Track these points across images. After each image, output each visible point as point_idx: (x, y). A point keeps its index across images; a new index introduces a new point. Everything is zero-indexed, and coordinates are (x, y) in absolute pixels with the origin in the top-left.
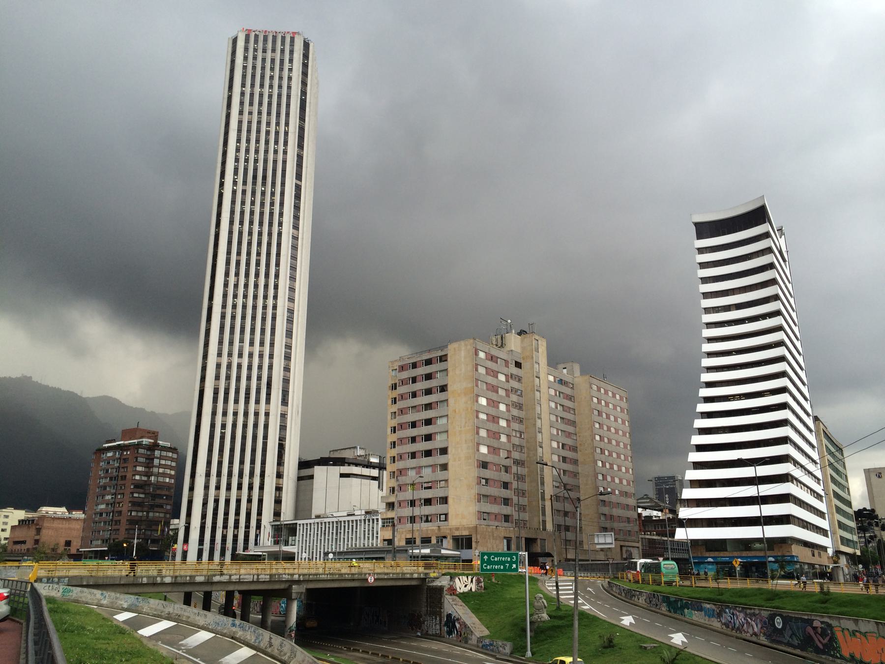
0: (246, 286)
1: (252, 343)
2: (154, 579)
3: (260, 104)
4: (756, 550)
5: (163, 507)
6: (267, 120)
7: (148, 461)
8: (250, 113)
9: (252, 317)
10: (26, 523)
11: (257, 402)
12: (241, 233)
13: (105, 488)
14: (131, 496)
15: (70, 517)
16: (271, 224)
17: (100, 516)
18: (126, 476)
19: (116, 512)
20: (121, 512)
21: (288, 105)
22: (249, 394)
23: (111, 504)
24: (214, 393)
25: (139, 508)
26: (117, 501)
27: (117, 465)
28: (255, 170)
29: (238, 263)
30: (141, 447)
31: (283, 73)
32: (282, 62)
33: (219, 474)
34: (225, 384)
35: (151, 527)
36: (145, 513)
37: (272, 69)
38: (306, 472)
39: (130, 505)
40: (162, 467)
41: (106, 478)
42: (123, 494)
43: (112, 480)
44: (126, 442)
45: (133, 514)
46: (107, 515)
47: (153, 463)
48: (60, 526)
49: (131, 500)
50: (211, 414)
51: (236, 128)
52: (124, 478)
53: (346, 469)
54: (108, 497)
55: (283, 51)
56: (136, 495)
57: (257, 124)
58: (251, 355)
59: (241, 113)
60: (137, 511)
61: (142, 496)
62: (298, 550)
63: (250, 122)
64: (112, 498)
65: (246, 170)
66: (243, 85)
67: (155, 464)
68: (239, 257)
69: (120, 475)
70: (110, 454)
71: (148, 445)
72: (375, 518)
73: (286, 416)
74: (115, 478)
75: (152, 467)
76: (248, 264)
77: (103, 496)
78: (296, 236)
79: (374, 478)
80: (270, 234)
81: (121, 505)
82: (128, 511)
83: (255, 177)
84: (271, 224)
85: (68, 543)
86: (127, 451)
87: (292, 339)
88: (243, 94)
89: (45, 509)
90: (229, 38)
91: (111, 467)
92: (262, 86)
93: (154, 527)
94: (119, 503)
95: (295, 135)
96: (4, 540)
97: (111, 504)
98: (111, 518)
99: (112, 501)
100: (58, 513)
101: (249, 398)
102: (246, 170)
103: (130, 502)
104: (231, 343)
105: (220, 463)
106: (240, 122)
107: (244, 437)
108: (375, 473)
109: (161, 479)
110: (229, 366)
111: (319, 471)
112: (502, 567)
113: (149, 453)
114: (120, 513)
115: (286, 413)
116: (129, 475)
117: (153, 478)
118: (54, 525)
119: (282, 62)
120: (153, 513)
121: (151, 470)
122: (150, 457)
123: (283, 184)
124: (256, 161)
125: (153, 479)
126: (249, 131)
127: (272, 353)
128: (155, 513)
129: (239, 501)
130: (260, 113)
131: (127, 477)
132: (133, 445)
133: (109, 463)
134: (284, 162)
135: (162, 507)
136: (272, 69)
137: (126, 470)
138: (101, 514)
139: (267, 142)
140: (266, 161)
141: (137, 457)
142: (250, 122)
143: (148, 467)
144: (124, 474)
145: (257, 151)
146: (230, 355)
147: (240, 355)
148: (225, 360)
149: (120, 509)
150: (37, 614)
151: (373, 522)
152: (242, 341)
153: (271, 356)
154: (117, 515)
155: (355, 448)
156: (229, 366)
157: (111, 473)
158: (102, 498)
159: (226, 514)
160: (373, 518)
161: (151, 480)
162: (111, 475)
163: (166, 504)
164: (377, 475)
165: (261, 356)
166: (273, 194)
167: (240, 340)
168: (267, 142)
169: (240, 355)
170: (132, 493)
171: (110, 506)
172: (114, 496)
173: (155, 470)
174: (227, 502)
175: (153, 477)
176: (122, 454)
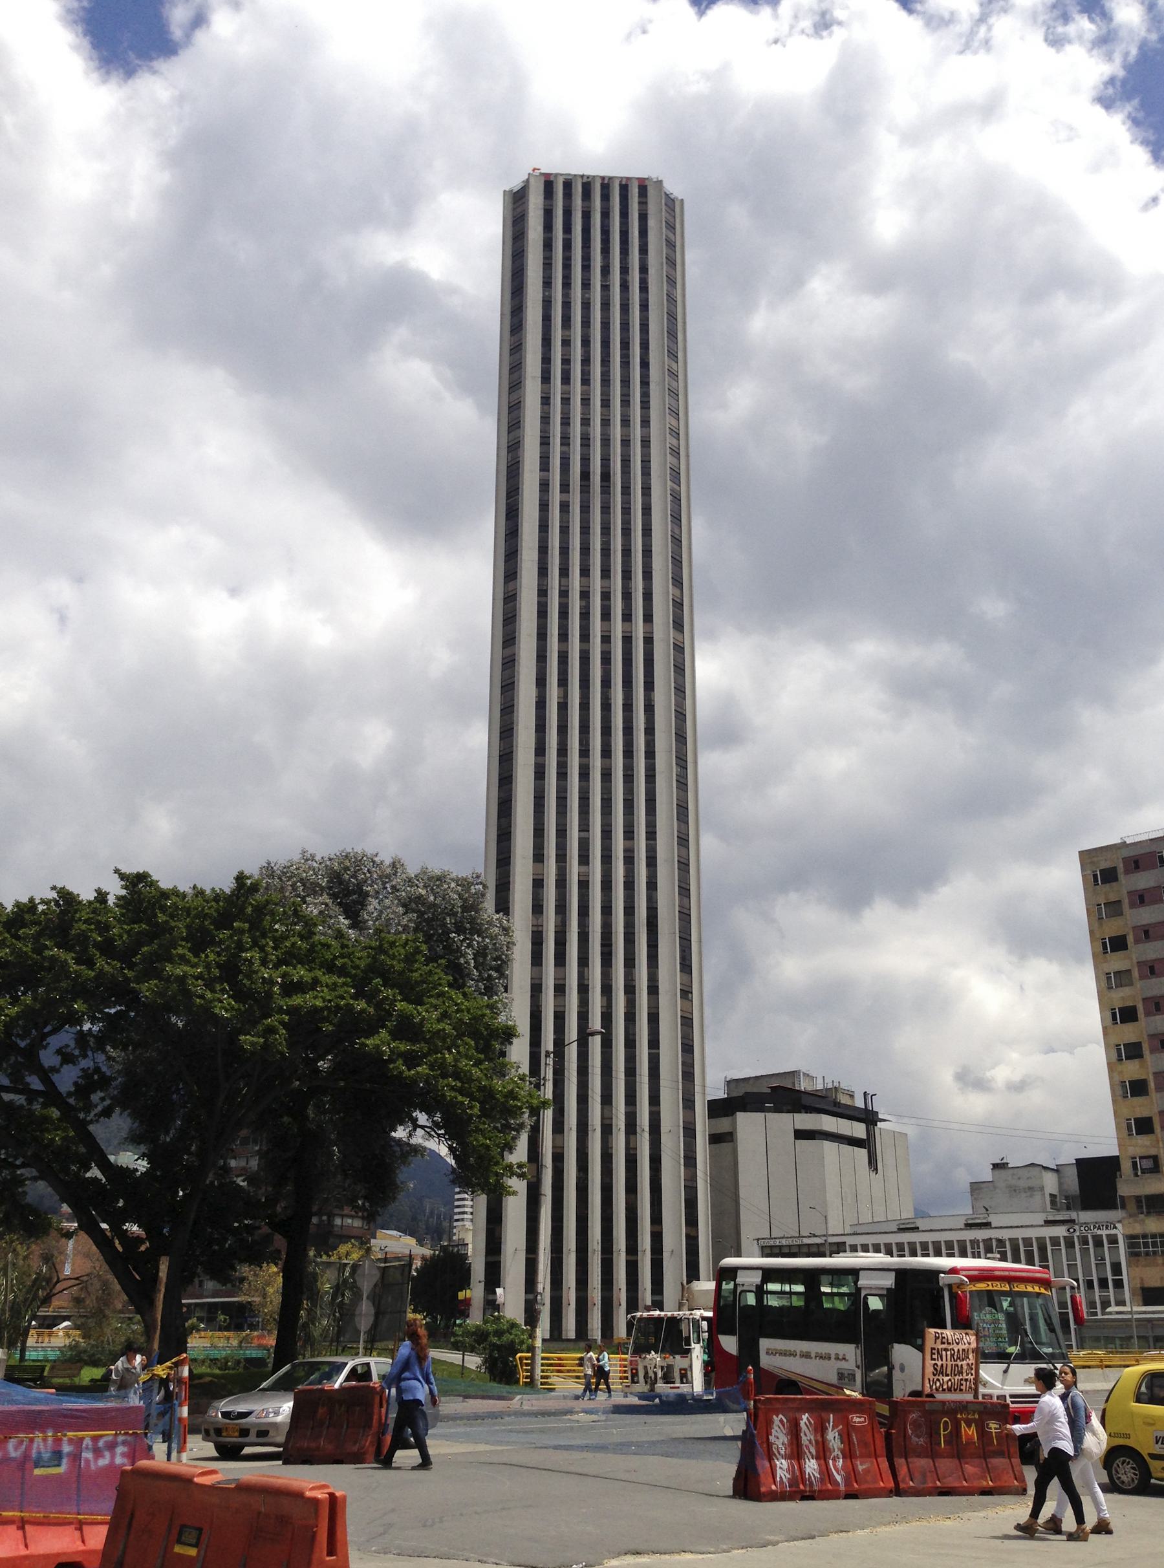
9: (557, 830)
24: (533, 944)
28: (586, 460)
36: (325, 1218)
38: (723, 1125)
53: (806, 1121)
72: (1104, 1232)
73: (690, 995)
78: (678, 600)
83: (585, 476)
105: (584, 827)
111: (748, 1124)
150: (330, 859)
151: (1085, 1252)
160: (1099, 1232)
164: (863, 1136)
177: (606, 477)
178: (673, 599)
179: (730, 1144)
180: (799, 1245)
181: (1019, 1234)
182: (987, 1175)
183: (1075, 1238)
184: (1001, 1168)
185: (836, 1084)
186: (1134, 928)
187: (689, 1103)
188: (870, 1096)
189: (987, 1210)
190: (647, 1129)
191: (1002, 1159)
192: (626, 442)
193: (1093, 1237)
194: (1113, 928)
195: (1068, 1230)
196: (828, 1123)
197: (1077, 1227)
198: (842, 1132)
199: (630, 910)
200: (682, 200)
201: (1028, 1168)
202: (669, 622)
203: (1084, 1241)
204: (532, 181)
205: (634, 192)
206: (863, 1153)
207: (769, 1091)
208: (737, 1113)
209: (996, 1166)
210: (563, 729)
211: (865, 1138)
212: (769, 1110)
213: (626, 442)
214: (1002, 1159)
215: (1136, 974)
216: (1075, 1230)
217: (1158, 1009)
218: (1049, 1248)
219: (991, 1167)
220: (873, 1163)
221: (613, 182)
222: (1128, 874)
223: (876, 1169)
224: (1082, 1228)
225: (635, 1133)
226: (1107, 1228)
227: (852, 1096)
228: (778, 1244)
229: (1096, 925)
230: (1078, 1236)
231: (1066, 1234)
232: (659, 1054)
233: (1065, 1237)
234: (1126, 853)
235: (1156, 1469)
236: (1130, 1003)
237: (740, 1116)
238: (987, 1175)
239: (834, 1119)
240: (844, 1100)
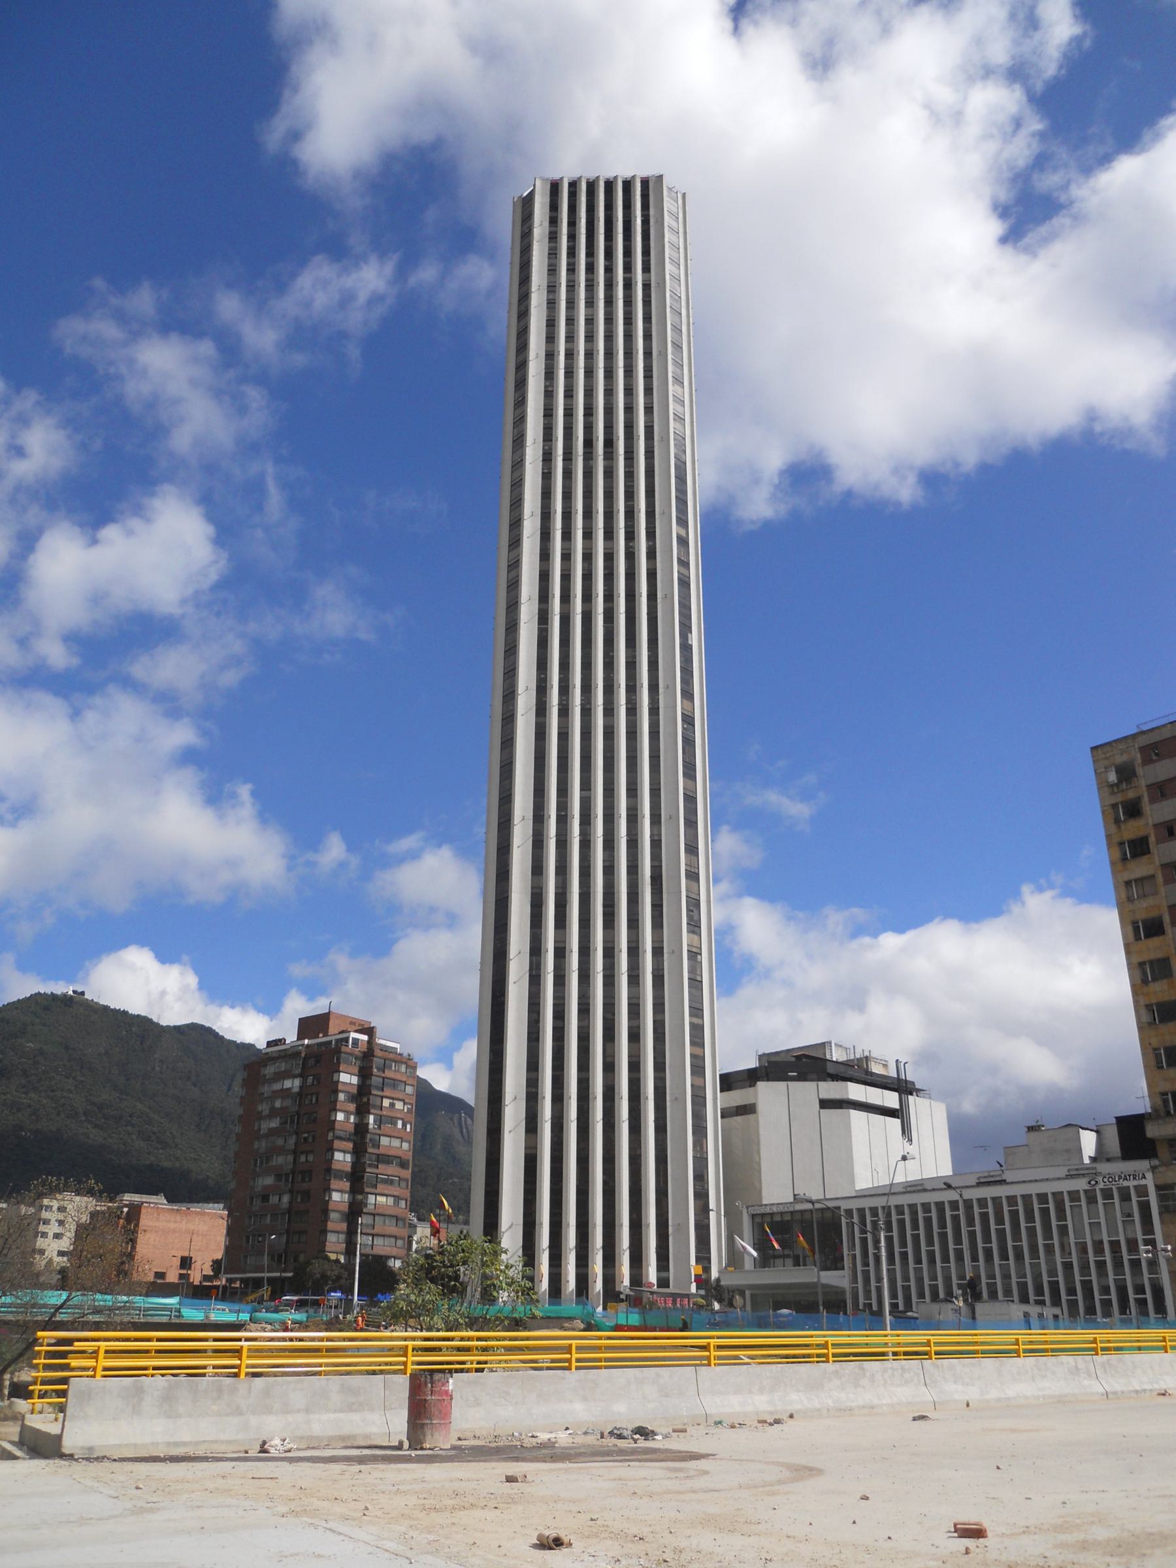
2: (812, 1214)
4: (976, 1269)
17: (262, 1202)
29: (590, 321)
38: (737, 1097)
48: (172, 1225)
53: (830, 1089)
62: (854, 1279)
72: (1131, 1183)
73: (699, 957)
83: (589, 443)
85: (186, 1262)
96: (58, 1256)
107: (569, 413)
108: (891, 1099)
111: (767, 1094)
118: (157, 1224)
154: (299, 1200)
160: (1126, 1183)
177: (609, 443)
180: (791, 1212)
181: (1034, 1189)
182: (1022, 1137)
183: (1098, 1191)
184: (1036, 1130)
185: (866, 1054)
186: (1155, 826)
187: (698, 1069)
188: (902, 1064)
189: (1001, 1166)
191: (1037, 1121)
193: (1119, 1189)
194: (1133, 829)
195: (1089, 1183)
196: (856, 1091)
197: (1100, 1179)
199: (633, 869)
201: (1065, 1129)
203: (1108, 1194)
206: (895, 1123)
207: (793, 1059)
208: (758, 1083)
209: (1031, 1129)
210: (565, 689)
211: (897, 1106)
214: (1037, 1121)
215: (1160, 878)
216: (1097, 1182)
217: (1171, 833)
218: (1067, 1204)
219: (1026, 1129)
220: (906, 1131)
222: (1153, 803)
223: (910, 1140)
224: (1105, 1180)
226: (1134, 1178)
227: (885, 1066)
229: (1113, 829)
230: (1102, 1190)
231: (1087, 1187)
233: (1086, 1191)
234: (1144, 741)
236: (1154, 914)
237: (760, 1085)
238: (1022, 1137)
239: (862, 1087)
240: (876, 1069)
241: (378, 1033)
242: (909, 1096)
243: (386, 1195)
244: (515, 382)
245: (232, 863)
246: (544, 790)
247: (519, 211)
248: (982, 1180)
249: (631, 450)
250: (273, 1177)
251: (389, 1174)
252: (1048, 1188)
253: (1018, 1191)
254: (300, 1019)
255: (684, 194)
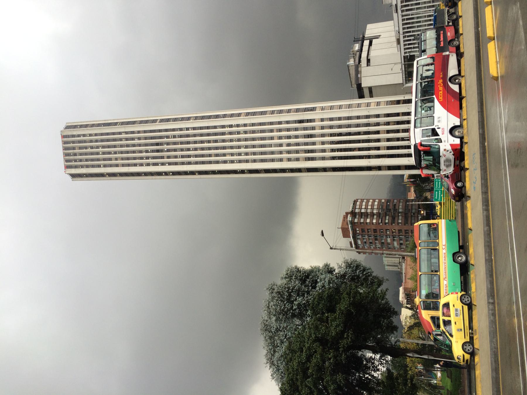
0: (232, 147)
1: (272, 138)
3: (109, 153)
5: (395, 204)
6: (119, 148)
7: (363, 217)
8: (116, 159)
10: (409, 300)
11: (313, 128)
12: (196, 156)
13: (383, 243)
14: (388, 224)
15: (405, 273)
16: (188, 136)
18: (374, 230)
19: (399, 234)
20: (399, 230)
21: (108, 134)
22: (308, 135)
23: (394, 237)
25: (396, 218)
26: (391, 234)
27: (366, 237)
28: (153, 151)
29: (217, 155)
30: (353, 221)
31: (87, 140)
32: (80, 142)
33: (369, 149)
34: (301, 153)
35: (410, 209)
36: (400, 214)
37: (86, 148)
38: (366, 92)
39: (394, 224)
40: (367, 207)
41: (375, 243)
42: (386, 230)
43: (377, 239)
44: (351, 233)
45: (401, 222)
46: (402, 240)
47: (364, 212)
49: (390, 224)
50: (324, 161)
51: (127, 168)
52: (375, 231)
54: (389, 240)
55: (73, 142)
56: (387, 221)
57: (123, 154)
58: (280, 138)
59: (117, 166)
60: (398, 219)
61: (387, 217)
63: (122, 159)
64: (389, 237)
65: (154, 158)
66: (99, 166)
67: (365, 212)
68: (212, 155)
69: (374, 234)
70: (359, 242)
71: (352, 217)
72: (412, 118)
74: (375, 237)
75: (367, 213)
76: (217, 148)
77: (388, 244)
78: (195, 118)
79: (371, 44)
80: (195, 135)
81: (395, 231)
82: (398, 225)
83: (158, 151)
84: (188, 136)
86: (356, 231)
87: (267, 111)
88: (105, 166)
89: (401, 299)
90: (72, 181)
91: (368, 240)
92: (98, 153)
93: (410, 208)
94: (393, 232)
95: (126, 127)
97: (394, 237)
98: (403, 237)
99: (392, 238)
100: (403, 296)
101: (311, 135)
102: (154, 158)
103: (392, 224)
104: (272, 153)
105: (360, 149)
106: (123, 165)
108: (366, 43)
109: (376, 207)
110: (289, 152)
112: (437, 182)
113: (357, 216)
114: (400, 231)
115: (321, 107)
116: (373, 227)
117: (375, 211)
119: (80, 142)
120: (399, 220)
121: (369, 213)
122: (360, 215)
123: (160, 131)
124: (147, 151)
125: (376, 212)
126: (128, 159)
127: (278, 123)
128: (400, 208)
129: (388, 132)
130: (115, 153)
131: (375, 228)
132: (352, 227)
133: (365, 242)
134: (145, 132)
135: (395, 205)
136: (86, 148)
137: (370, 230)
138: (401, 244)
139: (134, 145)
140: (146, 145)
141: (360, 222)
142: (122, 159)
143: (367, 216)
144: (373, 231)
145: (141, 152)
146: (281, 153)
147: (281, 145)
148: (285, 156)
149: (397, 231)
152: (270, 146)
153: (280, 123)
155: (348, 66)
156: (289, 152)
157: (372, 240)
158: (390, 244)
159: (398, 139)
161: (376, 212)
162: (374, 240)
163: (393, 202)
165: (280, 130)
166: (168, 137)
167: (270, 147)
168: (134, 145)
169: (281, 145)
170: (386, 223)
171: (395, 238)
172: (388, 236)
173: (369, 211)
174: (388, 140)
175: (374, 212)
176: (359, 234)
178: (195, 120)
179: (372, 88)
190: (368, 120)
192: (146, 138)
196: (364, 55)
198: (367, 49)
200: (66, 123)
202: (202, 121)
204: (67, 172)
205: (65, 139)
211: (369, 40)
212: (361, 75)
213: (146, 138)
220: (377, 37)
221: (64, 147)
225: (369, 123)
228: (405, 79)
232: (343, 117)
235: (408, 135)
241: (348, 211)
242: (365, 37)
243: (399, 206)
244: (138, 176)
245: (430, 146)
246: (264, 162)
247: (76, 179)
248: (395, 12)
249: (113, 133)
250: (394, 242)
251: (392, 205)
252: (400, 18)
253: (401, 27)
254: (343, 237)
255: (66, 123)
